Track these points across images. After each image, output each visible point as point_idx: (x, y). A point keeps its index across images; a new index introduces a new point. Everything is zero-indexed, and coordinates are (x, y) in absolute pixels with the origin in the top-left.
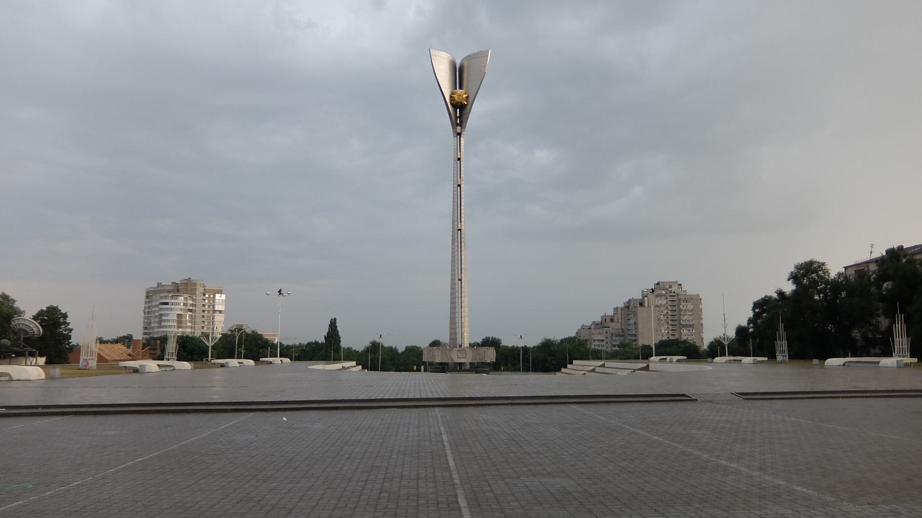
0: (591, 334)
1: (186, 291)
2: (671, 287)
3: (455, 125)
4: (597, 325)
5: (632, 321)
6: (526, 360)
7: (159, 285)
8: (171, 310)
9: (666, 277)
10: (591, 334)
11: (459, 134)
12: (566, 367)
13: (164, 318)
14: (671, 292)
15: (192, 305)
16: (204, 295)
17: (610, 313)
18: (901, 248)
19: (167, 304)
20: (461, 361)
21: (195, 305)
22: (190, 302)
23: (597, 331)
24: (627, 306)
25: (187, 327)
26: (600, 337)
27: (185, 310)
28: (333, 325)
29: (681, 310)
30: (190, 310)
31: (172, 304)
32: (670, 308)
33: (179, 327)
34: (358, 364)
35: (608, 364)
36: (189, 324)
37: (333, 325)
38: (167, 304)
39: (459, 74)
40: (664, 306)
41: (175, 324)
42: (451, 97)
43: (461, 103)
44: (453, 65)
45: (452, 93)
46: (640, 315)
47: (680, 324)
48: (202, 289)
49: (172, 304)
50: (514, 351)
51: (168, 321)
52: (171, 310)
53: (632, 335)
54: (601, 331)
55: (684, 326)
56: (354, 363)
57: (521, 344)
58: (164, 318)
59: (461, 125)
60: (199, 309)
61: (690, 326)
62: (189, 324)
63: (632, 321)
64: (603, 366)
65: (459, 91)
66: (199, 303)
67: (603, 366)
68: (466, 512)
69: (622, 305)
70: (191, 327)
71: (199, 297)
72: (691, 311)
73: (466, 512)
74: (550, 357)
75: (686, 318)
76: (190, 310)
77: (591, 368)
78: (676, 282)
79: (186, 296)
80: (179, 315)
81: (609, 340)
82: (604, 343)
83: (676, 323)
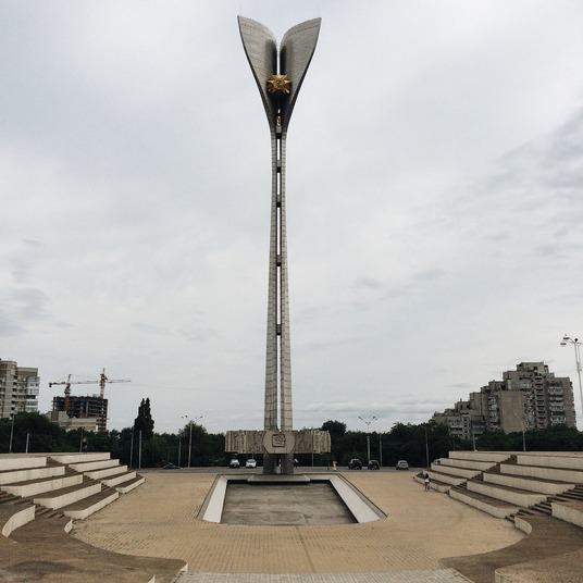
2: (535, 368)
3: (273, 123)
5: (494, 407)
6: (363, 449)
9: (531, 358)
12: (447, 457)
14: (536, 374)
17: (466, 399)
20: (278, 451)
24: (487, 391)
28: (145, 408)
32: (536, 393)
34: (113, 457)
37: (145, 408)
40: (529, 390)
42: (268, 84)
46: (503, 400)
48: (13, 372)
50: (359, 438)
56: (108, 455)
57: (368, 430)
63: (494, 407)
64: (512, 461)
72: (561, 396)
77: (457, 482)
78: (542, 363)
81: (468, 428)
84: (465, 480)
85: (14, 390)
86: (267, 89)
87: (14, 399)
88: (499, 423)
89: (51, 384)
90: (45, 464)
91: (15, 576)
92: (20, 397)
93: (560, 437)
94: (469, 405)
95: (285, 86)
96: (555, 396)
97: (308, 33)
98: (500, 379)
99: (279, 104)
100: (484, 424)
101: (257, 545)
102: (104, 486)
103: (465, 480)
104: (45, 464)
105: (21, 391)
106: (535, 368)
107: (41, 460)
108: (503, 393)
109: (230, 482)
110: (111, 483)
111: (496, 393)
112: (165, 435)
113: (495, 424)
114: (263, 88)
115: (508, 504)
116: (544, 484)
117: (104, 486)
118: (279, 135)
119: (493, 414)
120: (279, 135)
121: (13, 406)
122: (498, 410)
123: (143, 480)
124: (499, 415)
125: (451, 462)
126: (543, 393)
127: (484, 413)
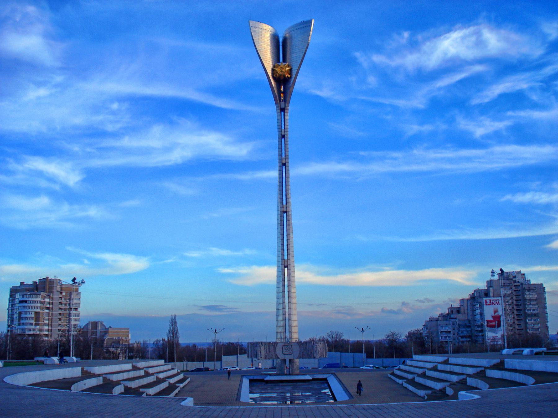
0: (437, 326)
1: (44, 290)
2: (515, 277)
4: (445, 317)
5: (478, 311)
7: (22, 284)
8: (31, 307)
10: (437, 326)
11: (283, 110)
13: (23, 316)
14: (515, 282)
15: (49, 303)
16: (61, 293)
17: (456, 305)
18: (431, 320)
19: (26, 302)
21: (52, 303)
22: (47, 300)
23: (445, 322)
24: (473, 298)
25: (44, 325)
26: (447, 329)
27: (42, 309)
29: (525, 299)
30: (48, 308)
31: (31, 302)
32: (514, 298)
33: (37, 324)
35: (452, 360)
36: (46, 322)
38: (26, 302)
39: (281, 47)
41: (33, 321)
42: (273, 70)
43: (284, 76)
44: (275, 38)
45: (274, 66)
47: (526, 313)
48: (59, 289)
49: (31, 302)
51: (26, 318)
52: (31, 307)
53: (478, 326)
54: (447, 322)
55: (529, 315)
58: (23, 316)
59: (285, 100)
60: (56, 307)
61: (535, 315)
62: (46, 322)
63: (478, 311)
64: (446, 362)
65: (282, 64)
66: (56, 302)
67: (446, 362)
68: (556, 198)
69: (467, 297)
70: (48, 325)
71: (56, 295)
72: (535, 300)
73: (556, 198)
74: (394, 349)
75: (530, 308)
76: (48, 308)
78: (520, 272)
79: (43, 294)
80: (37, 313)
82: (451, 335)
83: (522, 312)
84: (464, 377)
85: (61, 303)
87: (60, 311)
90: (131, 368)
91: (240, 271)
92: (65, 310)
93: (528, 337)
94: (458, 311)
96: (530, 300)
100: (470, 327)
101: (62, 312)
102: (157, 378)
103: (464, 377)
104: (131, 368)
105: (65, 304)
106: (515, 277)
107: (129, 366)
109: (251, 381)
110: (161, 376)
111: (479, 300)
112: (187, 346)
115: (430, 388)
117: (157, 378)
121: (60, 317)
123: (189, 380)
125: (414, 363)
126: (520, 298)
127: (470, 318)
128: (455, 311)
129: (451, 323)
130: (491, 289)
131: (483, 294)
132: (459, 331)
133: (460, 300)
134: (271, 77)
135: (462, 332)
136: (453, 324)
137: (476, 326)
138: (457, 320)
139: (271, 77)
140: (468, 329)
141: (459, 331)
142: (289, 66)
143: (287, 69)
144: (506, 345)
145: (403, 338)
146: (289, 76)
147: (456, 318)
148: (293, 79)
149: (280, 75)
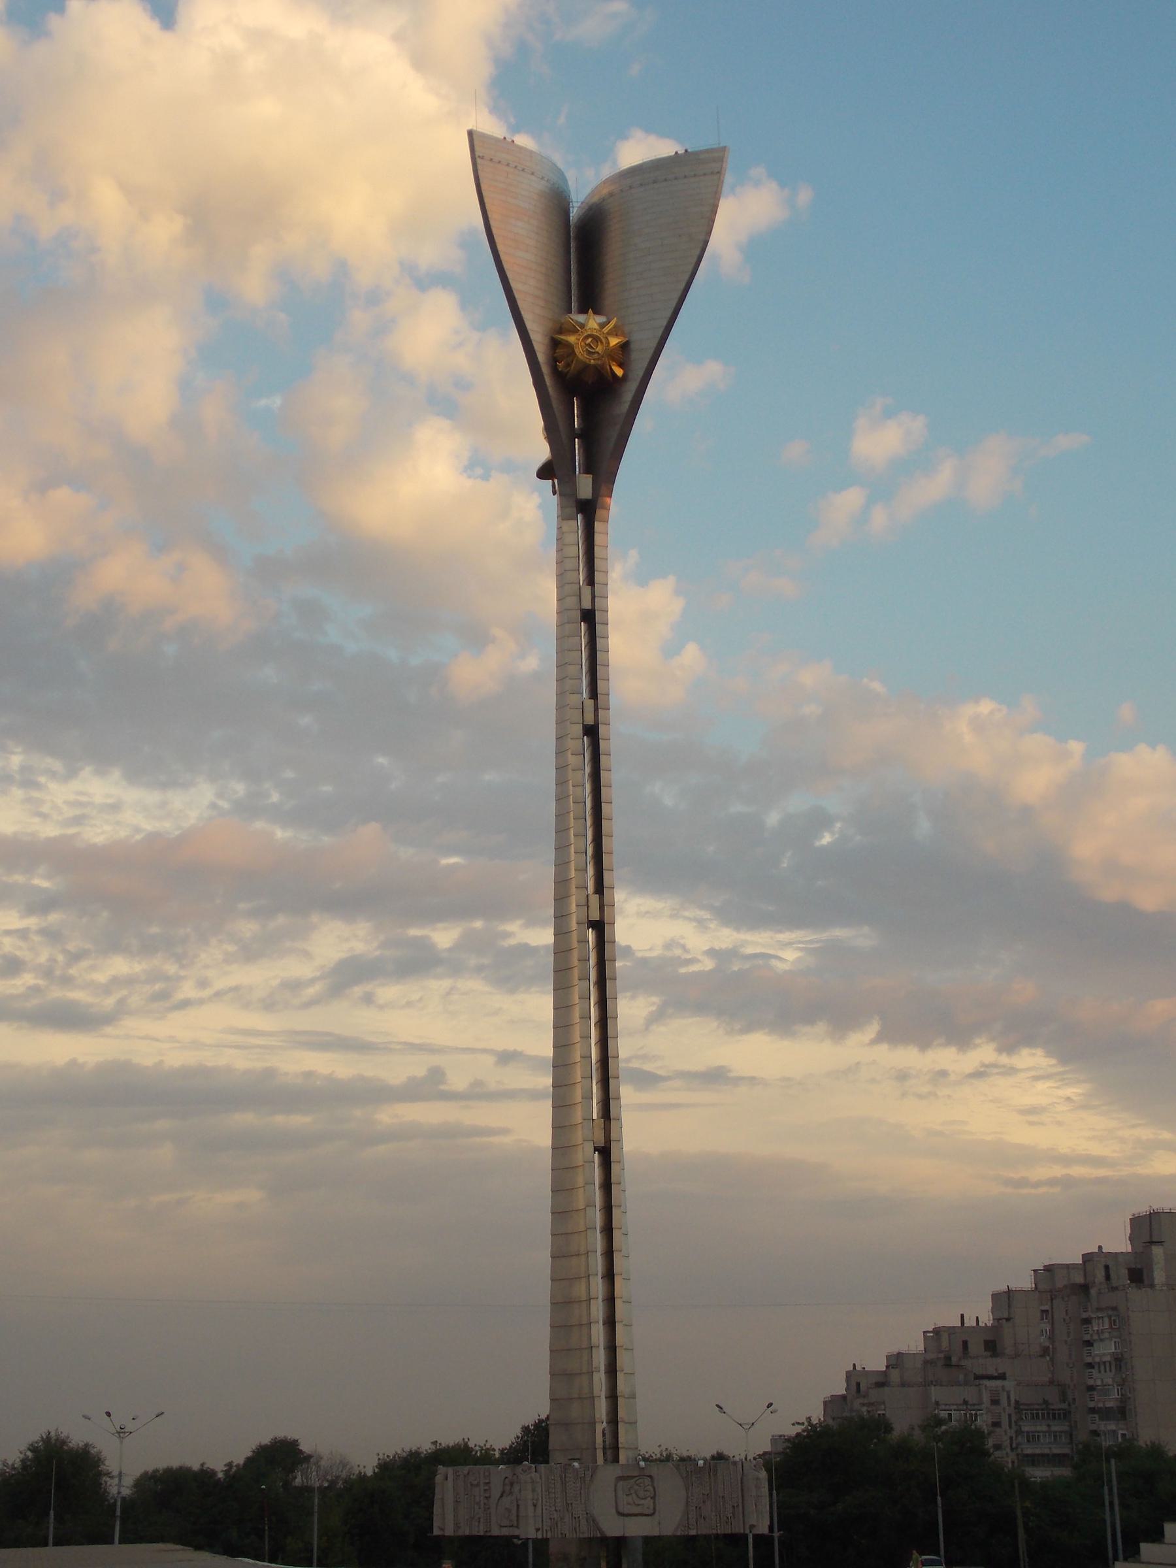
5: (1105, 1350)
42: (555, 344)
63: (1105, 1350)
86: (554, 361)
88: (1122, 1412)
89: (108, 1414)
91: (726, 937)
95: (611, 355)
97: (687, 187)
98: (1118, 1242)
99: (588, 412)
100: (1066, 1415)
108: (1136, 1295)
113: (1105, 1414)
114: (541, 357)
116: (530, 325)
118: (586, 512)
119: (1099, 1378)
120: (586, 512)
122: (1119, 1361)
124: (1122, 1383)
128: (976, 1347)
129: (986, 1398)
130: (1157, 1251)
131: (1124, 1272)
132: (1019, 1432)
133: (996, 1297)
134: (545, 370)
135: (1032, 1438)
136: (995, 1402)
137: (1093, 1410)
138: (1009, 1384)
139: (545, 370)
140: (1056, 1427)
141: (1019, 1432)
142: (615, 332)
143: (614, 341)
144: (315, 1561)
145: (370, 1473)
146: (619, 372)
147: (1002, 1377)
148: (631, 387)
149: (587, 367)
